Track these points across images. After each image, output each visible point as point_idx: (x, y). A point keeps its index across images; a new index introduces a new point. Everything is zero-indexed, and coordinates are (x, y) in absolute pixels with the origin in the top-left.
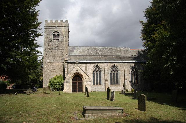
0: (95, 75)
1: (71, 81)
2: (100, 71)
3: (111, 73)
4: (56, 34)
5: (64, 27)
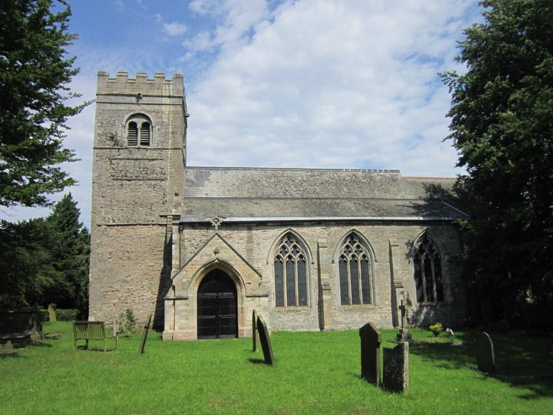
0: (285, 270)
1: (193, 293)
3: (343, 261)
4: (140, 122)
5: (169, 97)
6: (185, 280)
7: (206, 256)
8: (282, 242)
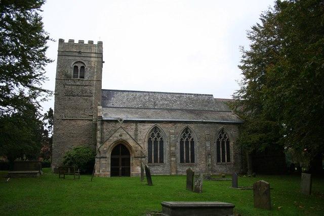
0: (153, 145)
1: (109, 155)
2: (161, 138)
3: (182, 143)
4: (79, 66)
6: (105, 149)
7: (116, 137)
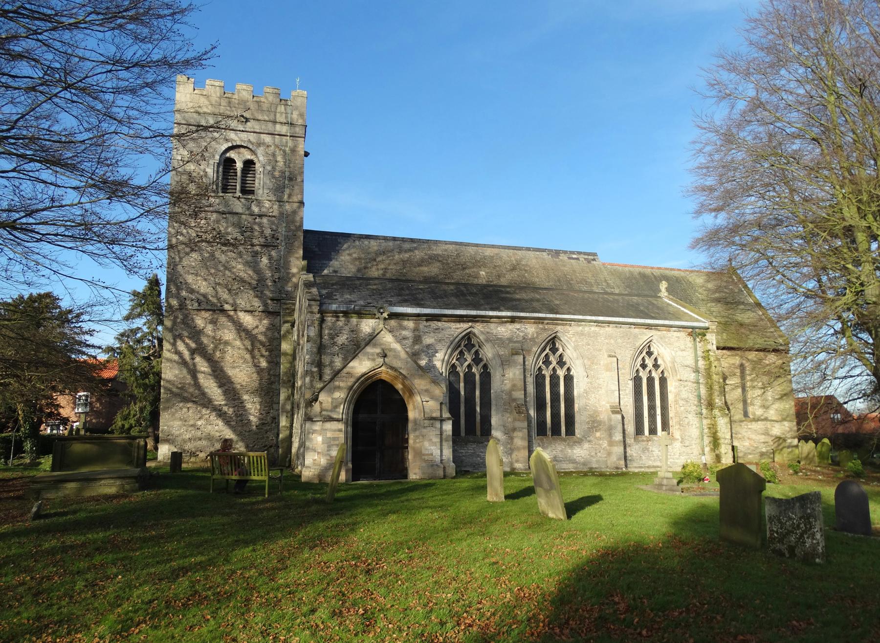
2: (485, 367)
8: (459, 346)
